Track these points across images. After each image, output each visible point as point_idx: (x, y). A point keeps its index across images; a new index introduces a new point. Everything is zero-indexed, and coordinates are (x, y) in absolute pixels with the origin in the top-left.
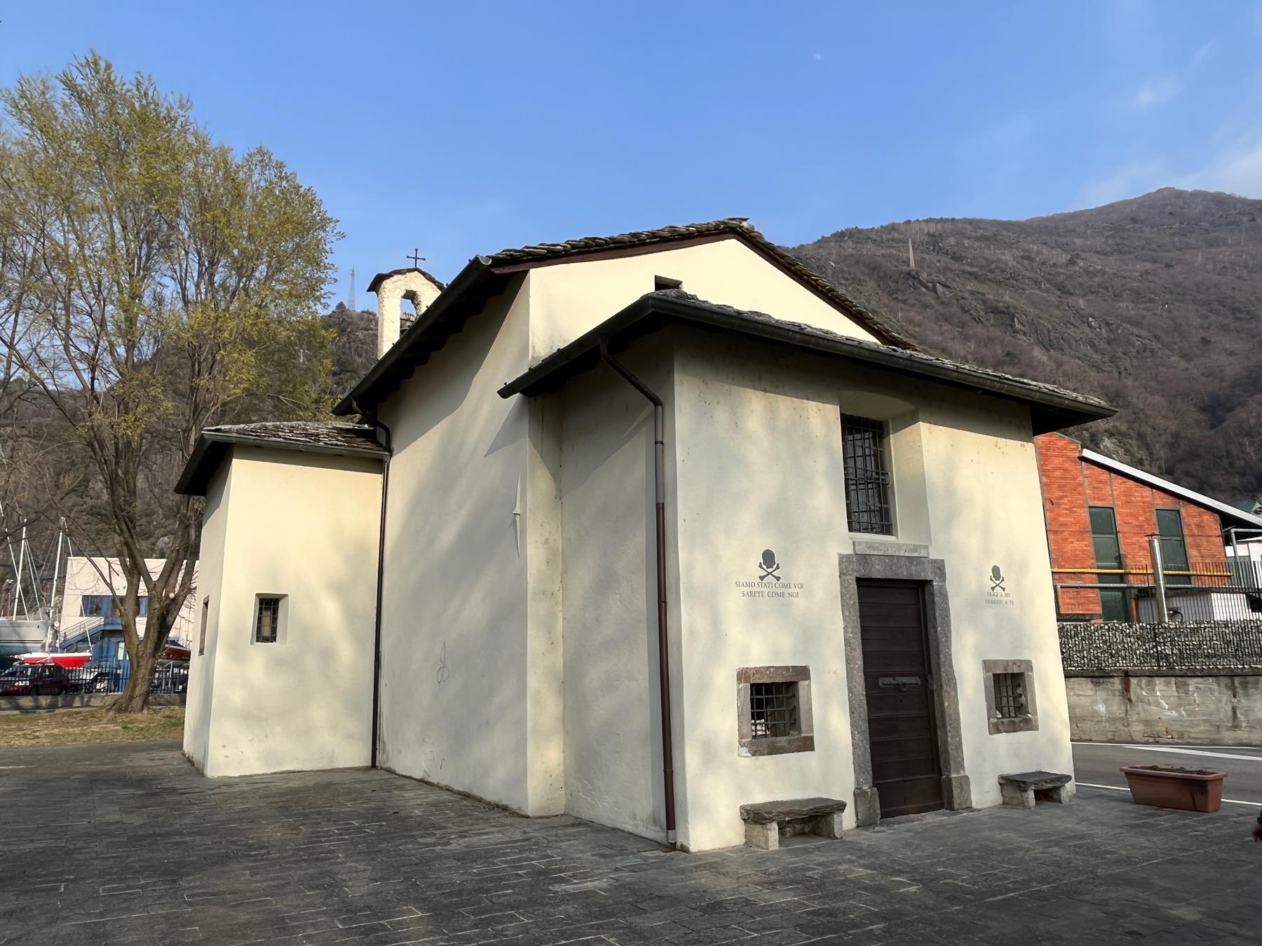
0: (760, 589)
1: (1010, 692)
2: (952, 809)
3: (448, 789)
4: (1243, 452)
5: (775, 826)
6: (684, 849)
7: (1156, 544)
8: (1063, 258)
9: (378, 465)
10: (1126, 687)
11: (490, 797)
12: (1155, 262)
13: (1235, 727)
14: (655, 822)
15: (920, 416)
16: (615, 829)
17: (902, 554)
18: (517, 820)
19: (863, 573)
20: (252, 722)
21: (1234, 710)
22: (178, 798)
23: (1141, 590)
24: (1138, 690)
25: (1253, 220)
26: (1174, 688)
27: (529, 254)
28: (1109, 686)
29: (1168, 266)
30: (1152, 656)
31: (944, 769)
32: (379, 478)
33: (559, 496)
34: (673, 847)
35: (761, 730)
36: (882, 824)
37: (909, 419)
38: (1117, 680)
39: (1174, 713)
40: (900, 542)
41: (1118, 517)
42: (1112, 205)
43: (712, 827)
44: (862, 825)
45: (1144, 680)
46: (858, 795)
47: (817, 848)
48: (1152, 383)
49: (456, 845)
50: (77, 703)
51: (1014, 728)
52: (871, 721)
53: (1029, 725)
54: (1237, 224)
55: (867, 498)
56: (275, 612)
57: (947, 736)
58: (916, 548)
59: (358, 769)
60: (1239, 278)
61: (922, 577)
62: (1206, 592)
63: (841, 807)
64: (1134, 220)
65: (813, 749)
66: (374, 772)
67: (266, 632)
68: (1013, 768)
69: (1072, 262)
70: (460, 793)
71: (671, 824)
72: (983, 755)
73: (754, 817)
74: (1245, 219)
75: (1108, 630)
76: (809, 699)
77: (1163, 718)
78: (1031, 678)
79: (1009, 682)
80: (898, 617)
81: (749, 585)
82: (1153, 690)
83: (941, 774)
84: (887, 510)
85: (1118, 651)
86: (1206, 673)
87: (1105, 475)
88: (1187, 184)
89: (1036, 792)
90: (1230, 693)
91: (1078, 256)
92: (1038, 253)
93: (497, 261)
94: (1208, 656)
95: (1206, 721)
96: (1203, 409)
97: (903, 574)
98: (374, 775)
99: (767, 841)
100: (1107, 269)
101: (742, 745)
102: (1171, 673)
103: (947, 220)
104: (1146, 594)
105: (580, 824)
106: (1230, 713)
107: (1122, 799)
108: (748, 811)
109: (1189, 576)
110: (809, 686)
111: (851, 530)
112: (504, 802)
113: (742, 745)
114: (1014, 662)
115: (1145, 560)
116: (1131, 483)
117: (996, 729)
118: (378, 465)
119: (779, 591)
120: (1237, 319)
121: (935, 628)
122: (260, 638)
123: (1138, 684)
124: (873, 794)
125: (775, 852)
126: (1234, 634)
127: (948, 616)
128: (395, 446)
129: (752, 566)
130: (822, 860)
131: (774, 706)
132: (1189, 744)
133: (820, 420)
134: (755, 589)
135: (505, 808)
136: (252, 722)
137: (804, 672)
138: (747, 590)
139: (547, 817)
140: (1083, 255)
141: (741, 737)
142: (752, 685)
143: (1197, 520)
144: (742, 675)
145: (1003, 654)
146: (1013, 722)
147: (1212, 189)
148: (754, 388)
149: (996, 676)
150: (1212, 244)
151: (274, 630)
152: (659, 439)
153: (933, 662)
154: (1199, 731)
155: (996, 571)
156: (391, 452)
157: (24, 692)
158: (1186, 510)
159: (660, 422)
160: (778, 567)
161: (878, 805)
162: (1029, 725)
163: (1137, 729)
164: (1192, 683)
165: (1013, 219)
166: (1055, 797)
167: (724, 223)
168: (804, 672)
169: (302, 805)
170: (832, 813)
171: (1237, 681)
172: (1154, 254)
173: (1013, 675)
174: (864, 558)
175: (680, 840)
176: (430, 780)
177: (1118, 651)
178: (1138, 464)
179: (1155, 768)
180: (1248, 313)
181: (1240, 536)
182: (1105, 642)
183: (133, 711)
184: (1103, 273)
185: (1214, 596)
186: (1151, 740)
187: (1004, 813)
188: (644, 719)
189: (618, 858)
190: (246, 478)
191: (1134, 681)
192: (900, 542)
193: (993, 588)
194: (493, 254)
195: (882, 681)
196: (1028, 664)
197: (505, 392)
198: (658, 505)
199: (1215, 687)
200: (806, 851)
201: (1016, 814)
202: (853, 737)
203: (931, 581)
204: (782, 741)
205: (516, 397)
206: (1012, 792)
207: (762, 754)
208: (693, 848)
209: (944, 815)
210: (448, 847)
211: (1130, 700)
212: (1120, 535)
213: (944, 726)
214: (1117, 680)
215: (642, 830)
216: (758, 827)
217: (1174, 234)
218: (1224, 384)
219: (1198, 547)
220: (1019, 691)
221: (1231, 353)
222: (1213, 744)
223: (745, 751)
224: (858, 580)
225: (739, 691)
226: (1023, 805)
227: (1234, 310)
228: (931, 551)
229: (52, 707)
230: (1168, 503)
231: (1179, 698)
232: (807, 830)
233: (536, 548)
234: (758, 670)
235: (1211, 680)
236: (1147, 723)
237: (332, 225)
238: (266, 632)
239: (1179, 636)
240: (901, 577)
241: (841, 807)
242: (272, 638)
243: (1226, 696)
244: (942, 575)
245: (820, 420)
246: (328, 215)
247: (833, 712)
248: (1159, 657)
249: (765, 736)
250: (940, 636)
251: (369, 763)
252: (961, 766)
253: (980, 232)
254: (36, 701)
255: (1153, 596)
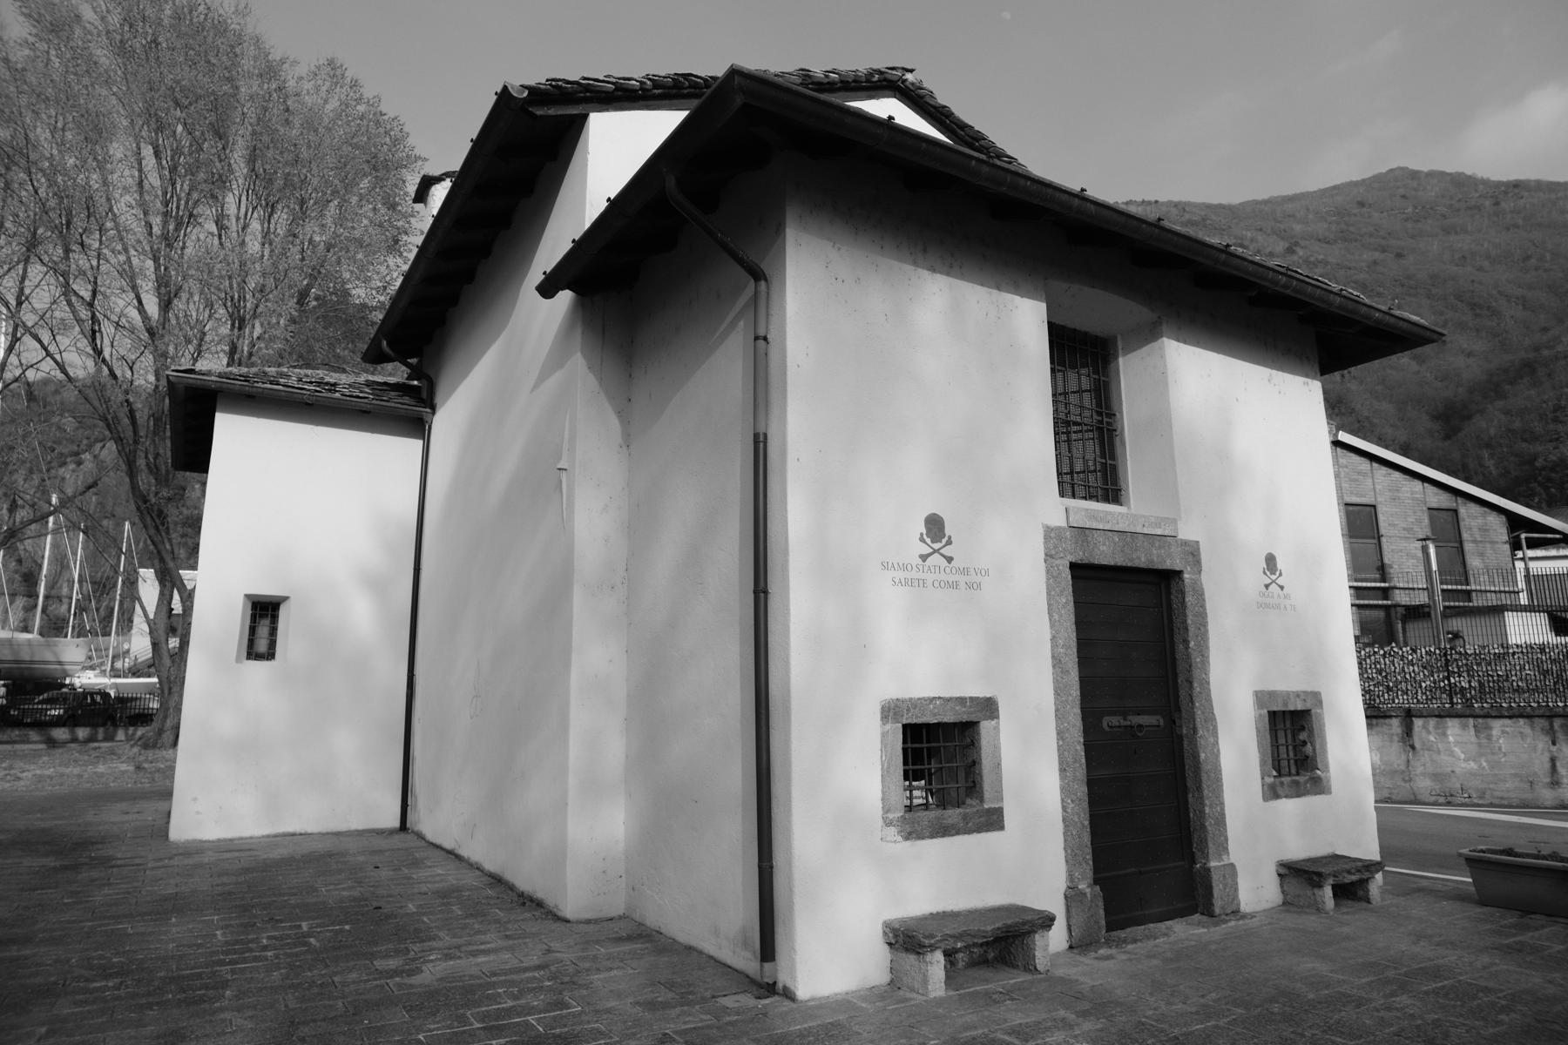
0: (921, 575)
1: (1292, 738)
2: (1211, 915)
3: (478, 868)
4: (1481, 466)
5: (939, 956)
6: (788, 995)
7: (1432, 550)
8: (1280, 247)
9: (417, 425)
10: (1408, 731)
11: (523, 885)
12: (1384, 251)
13: (1555, 783)
14: (745, 944)
15: (1164, 327)
16: (690, 949)
17: (1139, 530)
18: (558, 926)
19: (1079, 556)
20: (253, 770)
21: (1553, 760)
22: (190, 861)
23: (1407, 608)
24: (1424, 734)
25: (1497, 204)
26: (1472, 732)
27: (587, 88)
28: (1385, 729)
29: (1399, 256)
30: (1443, 690)
31: (1198, 854)
32: (416, 445)
33: (628, 440)
34: (770, 989)
35: (919, 796)
36: (1108, 943)
37: (1149, 334)
38: (1395, 722)
39: (1473, 765)
40: (1138, 510)
41: (1381, 518)
42: (1335, 187)
43: (834, 953)
44: (1079, 945)
45: (1432, 722)
46: (1072, 897)
47: (1008, 994)
48: (1379, 388)
49: (432, 972)
50: (121, 735)
51: (1298, 791)
52: (1091, 783)
53: (1318, 786)
54: (1478, 208)
55: (1088, 451)
56: (275, 618)
57: (1203, 805)
58: (1159, 522)
59: (380, 833)
60: (1480, 269)
61: (1168, 564)
62: (1498, 610)
63: (1047, 921)
64: (1361, 204)
65: (1002, 828)
66: (402, 836)
67: (262, 646)
68: (1298, 850)
69: (1290, 250)
70: (491, 875)
71: (768, 950)
72: (1256, 833)
73: (906, 940)
74: (1487, 203)
75: (1384, 656)
76: (997, 748)
77: (1458, 770)
78: (1320, 717)
79: (1288, 724)
80: (1132, 623)
81: (905, 568)
82: (1445, 734)
83: (1194, 862)
84: (1114, 468)
85: (1397, 683)
86: (1516, 712)
87: (1364, 464)
88: (1423, 160)
89: (1334, 887)
90: (1548, 739)
91: (1296, 244)
92: (1252, 240)
93: (537, 95)
94: (1518, 690)
95: (1516, 775)
96: (1436, 417)
97: (1141, 560)
98: (399, 841)
99: (925, 981)
100: (1330, 259)
101: (888, 823)
102: (1468, 712)
103: (1149, 203)
104: (1416, 613)
105: (640, 936)
106: (1547, 765)
107: (1459, 896)
108: (895, 932)
109: (1469, 593)
110: (997, 728)
111: (1062, 494)
112: (540, 895)
113: (888, 823)
114: (1297, 695)
115: (1411, 567)
116: (1397, 475)
117: (1272, 793)
118: (417, 425)
119: (951, 578)
120: (1477, 315)
121: (1186, 642)
122: (252, 654)
123: (1424, 727)
124: (1094, 896)
125: (939, 1002)
126: (1553, 661)
127: (1205, 625)
128: (438, 400)
129: (913, 543)
130: (1018, 1019)
131: (940, 758)
132: (1491, 805)
133: (1025, 320)
134: (914, 574)
135: (539, 904)
136: (253, 770)
137: (989, 707)
138: (900, 575)
139: (596, 921)
140: (1302, 243)
141: (886, 810)
142: (905, 727)
143: (1480, 521)
144: (890, 711)
145: (1289, 682)
146: (1297, 783)
147: (1450, 168)
148: (915, 263)
149: (1273, 715)
150: (1447, 231)
151: (272, 644)
152: (761, 333)
153: (1182, 693)
154: (1510, 788)
155: (1271, 561)
156: (433, 409)
157: (58, 722)
158: (1467, 511)
159: (762, 311)
160: (949, 542)
161: (1102, 912)
162: (1318, 786)
163: (1423, 785)
164: (1497, 725)
165: (1224, 202)
166: (1361, 893)
167: (880, 72)
168: (989, 707)
169: (270, 888)
170: (1031, 932)
171: (1557, 723)
172: (1383, 242)
173: (1293, 713)
174: (1082, 533)
175: (783, 979)
176: (464, 853)
177: (1397, 683)
178: (1405, 452)
179: (1509, 852)
180: (1489, 308)
181: (1533, 544)
182: (1380, 672)
183: (163, 747)
184: (1326, 263)
185: (1509, 616)
186: (1442, 800)
187: (1292, 920)
188: (736, 777)
189: (674, 1012)
190: (232, 434)
191: (1418, 723)
192: (1138, 510)
193: (1267, 586)
194: (532, 82)
195: (1106, 721)
196: (1316, 697)
197: (548, 289)
198: (756, 436)
199: (1527, 730)
200: (990, 999)
201: (1311, 921)
202: (1064, 809)
203: (1180, 573)
204: (953, 815)
205: (565, 297)
206: (1295, 886)
207: (921, 837)
208: (803, 991)
209: (1199, 924)
210: (416, 980)
211: (1413, 747)
212: (1383, 540)
213: (1199, 788)
214: (1395, 722)
215: (728, 955)
216: (912, 957)
217: (1406, 220)
218: (1460, 390)
219: (1482, 555)
220: (1303, 736)
221: (1469, 355)
222: (1524, 806)
223: (892, 831)
224: (1073, 566)
225: (884, 735)
226: (1318, 909)
227: (1473, 306)
228: (1180, 525)
229: (92, 739)
230: (1443, 500)
231: (1480, 745)
232: (991, 955)
233: (592, 519)
234: (914, 704)
235: (1522, 721)
236: (1436, 777)
237: (420, 163)
238: (262, 646)
239: (1478, 664)
240: (1136, 564)
241: (1047, 921)
242: (270, 655)
243: (1542, 743)
244: (1197, 563)
245: (1025, 320)
246: (417, 152)
247: (1033, 764)
248: (1452, 691)
249: (926, 806)
250: (1194, 654)
251: (397, 824)
252: (1223, 848)
253: (1187, 216)
254: (73, 733)
255: (1429, 615)
